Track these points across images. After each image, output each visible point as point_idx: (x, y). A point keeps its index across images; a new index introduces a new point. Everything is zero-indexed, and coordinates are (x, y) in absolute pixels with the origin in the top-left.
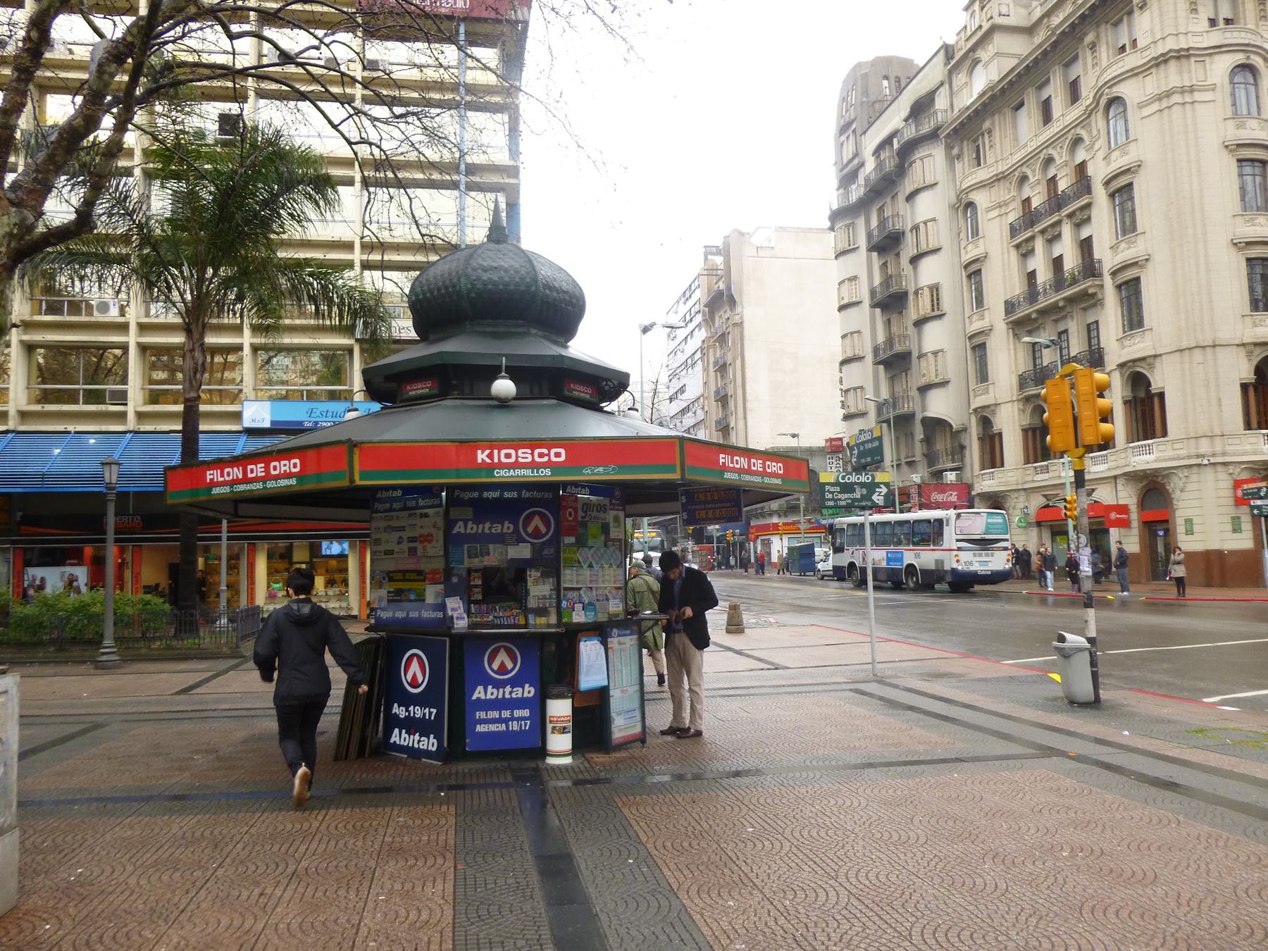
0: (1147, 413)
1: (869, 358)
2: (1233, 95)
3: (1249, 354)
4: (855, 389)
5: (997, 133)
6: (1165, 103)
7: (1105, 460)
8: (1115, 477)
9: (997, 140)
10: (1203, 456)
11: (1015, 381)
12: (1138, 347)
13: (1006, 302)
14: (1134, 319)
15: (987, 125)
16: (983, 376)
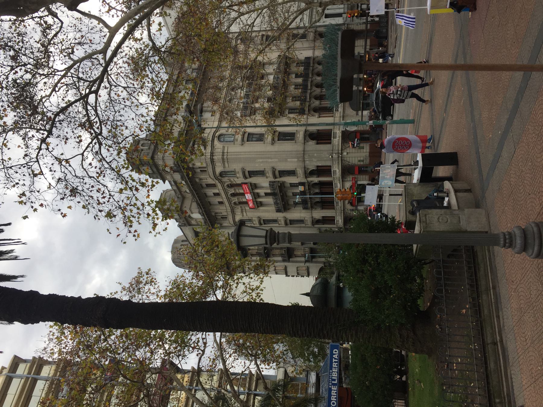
0: (324, 171)
1: (286, 264)
2: (227, 142)
3: (308, 141)
4: (297, 270)
5: (217, 211)
6: (226, 161)
7: (336, 184)
8: (342, 181)
9: (219, 211)
10: (339, 156)
11: (304, 211)
12: (300, 172)
13: (277, 212)
14: (292, 173)
15: (213, 214)
16: (301, 221)
